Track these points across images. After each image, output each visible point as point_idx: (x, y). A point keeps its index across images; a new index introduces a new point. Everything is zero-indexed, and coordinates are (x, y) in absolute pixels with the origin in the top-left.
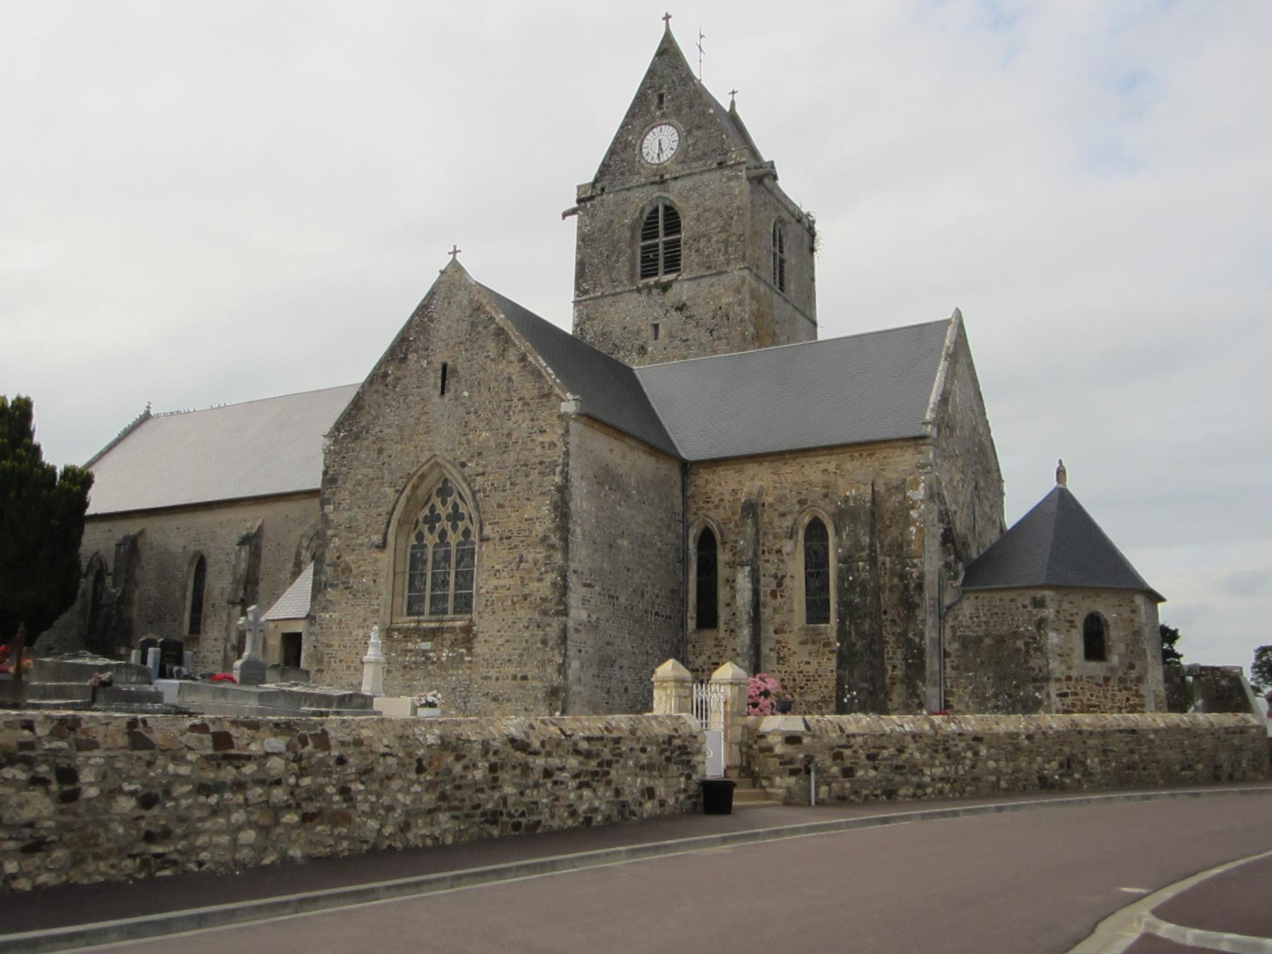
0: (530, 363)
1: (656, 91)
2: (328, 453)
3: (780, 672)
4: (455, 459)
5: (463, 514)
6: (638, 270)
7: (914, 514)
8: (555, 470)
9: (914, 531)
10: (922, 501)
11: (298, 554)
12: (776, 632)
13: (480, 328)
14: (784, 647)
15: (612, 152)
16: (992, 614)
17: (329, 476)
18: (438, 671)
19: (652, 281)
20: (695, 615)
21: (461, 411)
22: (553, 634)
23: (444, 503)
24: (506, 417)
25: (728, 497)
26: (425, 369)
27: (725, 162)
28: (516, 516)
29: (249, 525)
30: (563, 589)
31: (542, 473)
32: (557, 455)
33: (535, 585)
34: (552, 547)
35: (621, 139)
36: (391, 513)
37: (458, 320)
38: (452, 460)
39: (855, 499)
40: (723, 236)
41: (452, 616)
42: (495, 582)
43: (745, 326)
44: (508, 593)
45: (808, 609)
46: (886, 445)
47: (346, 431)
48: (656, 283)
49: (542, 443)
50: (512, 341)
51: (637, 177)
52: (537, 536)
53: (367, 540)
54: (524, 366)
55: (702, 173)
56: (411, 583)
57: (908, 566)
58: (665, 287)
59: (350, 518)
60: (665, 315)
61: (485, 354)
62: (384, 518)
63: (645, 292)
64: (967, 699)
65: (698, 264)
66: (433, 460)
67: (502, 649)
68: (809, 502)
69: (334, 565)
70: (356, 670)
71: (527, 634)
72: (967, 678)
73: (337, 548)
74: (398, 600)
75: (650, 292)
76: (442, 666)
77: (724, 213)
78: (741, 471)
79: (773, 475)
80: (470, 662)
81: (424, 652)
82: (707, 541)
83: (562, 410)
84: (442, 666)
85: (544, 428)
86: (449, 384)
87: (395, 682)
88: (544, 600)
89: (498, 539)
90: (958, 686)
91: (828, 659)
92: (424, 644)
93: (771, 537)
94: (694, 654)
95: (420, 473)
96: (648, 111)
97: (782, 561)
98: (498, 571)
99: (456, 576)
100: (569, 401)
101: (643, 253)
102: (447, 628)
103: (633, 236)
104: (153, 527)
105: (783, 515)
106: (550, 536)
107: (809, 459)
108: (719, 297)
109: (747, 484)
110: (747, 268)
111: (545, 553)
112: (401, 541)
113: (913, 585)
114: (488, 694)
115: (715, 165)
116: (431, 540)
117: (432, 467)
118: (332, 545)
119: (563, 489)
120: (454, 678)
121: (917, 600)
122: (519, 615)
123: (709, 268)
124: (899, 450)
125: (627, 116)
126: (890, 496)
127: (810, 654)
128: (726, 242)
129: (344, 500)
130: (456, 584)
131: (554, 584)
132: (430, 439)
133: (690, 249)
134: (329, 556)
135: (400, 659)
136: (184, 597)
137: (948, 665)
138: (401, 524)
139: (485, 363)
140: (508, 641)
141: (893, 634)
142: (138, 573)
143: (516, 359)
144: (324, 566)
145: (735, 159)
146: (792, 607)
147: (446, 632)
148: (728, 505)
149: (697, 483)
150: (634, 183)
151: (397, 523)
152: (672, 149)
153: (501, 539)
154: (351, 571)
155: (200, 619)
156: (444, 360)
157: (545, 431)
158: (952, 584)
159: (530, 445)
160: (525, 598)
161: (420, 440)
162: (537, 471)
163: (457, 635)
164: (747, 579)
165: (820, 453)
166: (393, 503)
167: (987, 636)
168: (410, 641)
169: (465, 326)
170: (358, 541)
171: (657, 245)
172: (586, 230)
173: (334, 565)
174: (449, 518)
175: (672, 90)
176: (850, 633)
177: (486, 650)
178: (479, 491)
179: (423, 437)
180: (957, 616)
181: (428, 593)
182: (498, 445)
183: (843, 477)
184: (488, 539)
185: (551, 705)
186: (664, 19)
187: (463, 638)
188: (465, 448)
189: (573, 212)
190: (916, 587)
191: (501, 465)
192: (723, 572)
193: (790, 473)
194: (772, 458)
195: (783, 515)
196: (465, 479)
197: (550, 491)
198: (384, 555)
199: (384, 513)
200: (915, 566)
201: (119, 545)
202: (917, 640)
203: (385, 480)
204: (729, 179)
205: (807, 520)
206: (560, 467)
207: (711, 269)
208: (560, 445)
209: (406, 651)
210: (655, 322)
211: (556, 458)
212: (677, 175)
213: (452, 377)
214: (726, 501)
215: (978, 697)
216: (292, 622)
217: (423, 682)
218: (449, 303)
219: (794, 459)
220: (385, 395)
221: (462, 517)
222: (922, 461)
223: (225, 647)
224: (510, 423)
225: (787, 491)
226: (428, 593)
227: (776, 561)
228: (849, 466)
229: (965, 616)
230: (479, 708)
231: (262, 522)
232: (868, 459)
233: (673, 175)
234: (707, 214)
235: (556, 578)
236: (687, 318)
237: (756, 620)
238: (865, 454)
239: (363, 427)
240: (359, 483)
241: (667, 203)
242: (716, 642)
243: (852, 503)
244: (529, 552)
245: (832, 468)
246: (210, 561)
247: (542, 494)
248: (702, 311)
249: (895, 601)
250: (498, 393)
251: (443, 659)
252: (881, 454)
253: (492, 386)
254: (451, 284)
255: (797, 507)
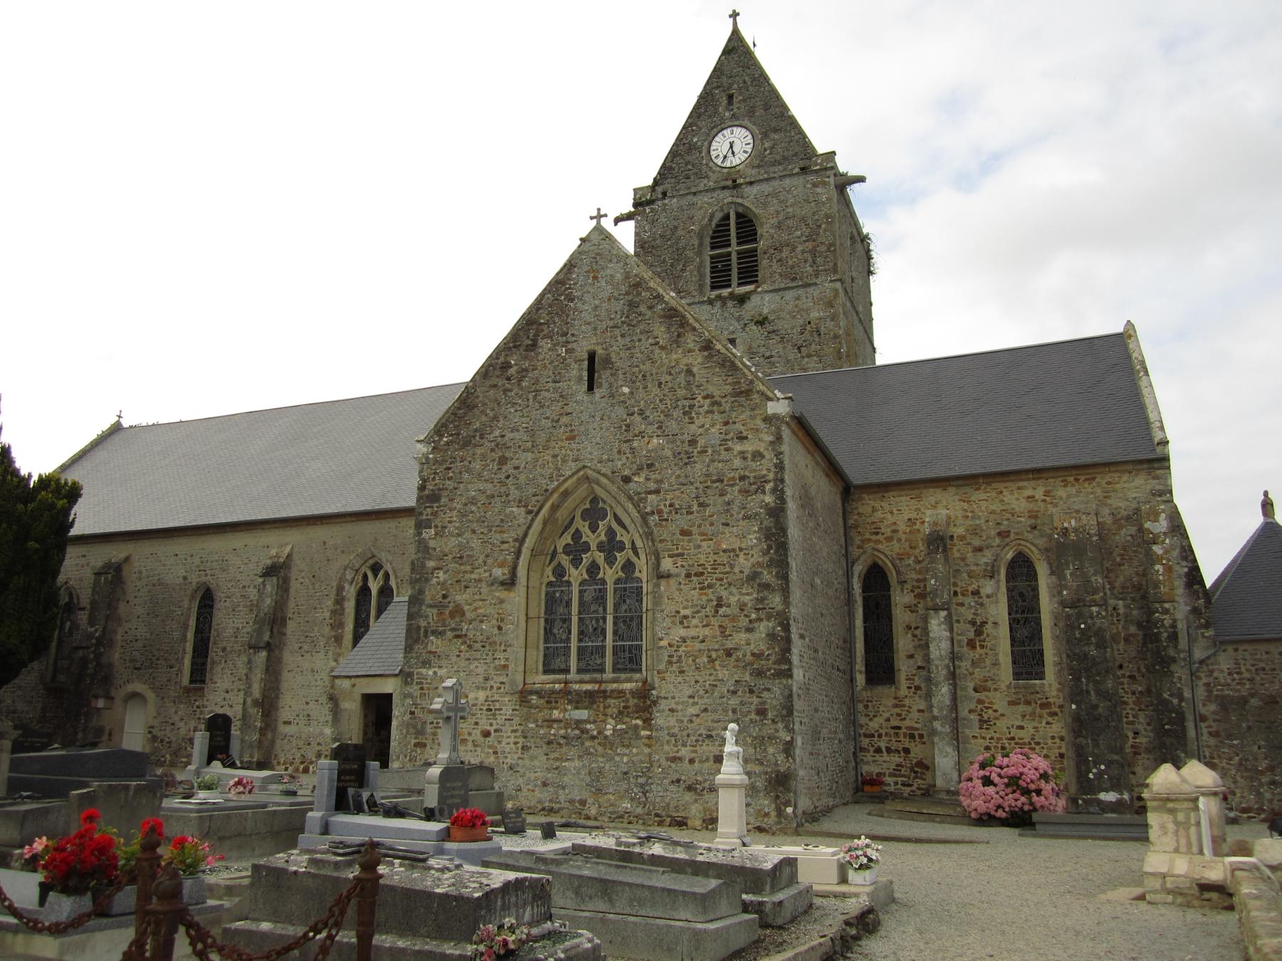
0: (719, 351)
1: (724, 91)
2: (424, 462)
3: (984, 738)
4: (613, 473)
5: (622, 542)
6: (708, 281)
7: (1157, 549)
8: (764, 487)
9: (1161, 570)
10: (1165, 533)
11: (340, 589)
12: (976, 690)
13: (643, 308)
14: (987, 708)
15: (674, 153)
16: (1257, 670)
17: (427, 492)
18: (600, 749)
19: (725, 292)
20: (863, 669)
21: (620, 412)
22: (774, 703)
23: (594, 528)
24: (687, 420)
25: (902, 527)
26: (565, 359)
27: (810, 166)
28: (709, 547)
29: (273, 552)
30: (783, 643)
31: (745, 492)
32: (765, 467)
33: (743, 636)
34: (766, 586)
35: (685, 141)
36: (521, 541)
37: (609, 300)
38: (609, 473)
39: (1076, 530)
40: (810, 245)
41: (611, 675)
42: (682, 632)
43: (840, 343)
44: (703, 646)
45: (1014, 663)
46: (1112, 469)
47: (452, 435)
48: (731, 294)
49: (742, 452)
50: (689, 324)
51: (705, 181)
52: (741, 572)
53: (487, 574)
54: (710, 356)
55: (781, 178)
56: (548, 632)
57: (1158, 612)
58: (742, 300)
59: (460, 545)
60: (743, 329)
61: (651, 341)
62: (511, 546)
63: (718, 304)
64: (1233, 772)
65: (781, 275)
66: (582, 473)
67: (697, 721)
68: (1012, 535)
69: (439, 606)
70: (475, 746)
71: (734, 702)
72: (1231, 746)
73: (442, 584)
74: (532, 653)
75: (724, 304)
76: (606, 742)
77: (810, 221)
78: (918, 497)
79: (962, 503)
80: (649, 737)
81: (578, 722)
82: (876, 580)
83: (770, 411)
84: (606, 742)
85: (744, 434)
86: (600, 377)
87: (536, 763)
88: (758, 656)
89: (683, 575)
90: (1219, 757)
91: (1048, 723)
92: (577, 712)
93: (965, 575)
94: (867, 715)
95: (562, 489)
96: (716, 112)
97: (982, 605)
98: (685, 617)
99: (615, 624)
100: (778, 399)
101: (712, 263)
102: (612, 691)
103: (701, 245)
104: (143, 558)
105: (979, 549)
106: (762, 573)
107: (1008, 484)
108: (807, 310)
109: (928, 512)
110: (840, 280)
111: (755, 596)
112: (535, 576)
113: (1165, 635)
114: (678, 781)
115: (797, 170)
116: (576, 575)
117: (579, 482)
118: (435, 580)
119: (777, 512)
120: (625, 759)
121: (1171, 652)
122: (720, 676)
123: (794, 279)
124: (1127, 475)
125: (690, 116)
126: (1120, 527)
127: (1024, 716)
128: (813, 252)
129: (449, 522)
130: (615, 633)
131: (772, 636)
132: (574, 446)
133: (770, 259)
134: (432, 593)
135: (542, 732)
136: (184, 639)
137: (1205, 731)
138: (534, 554)
139: (652, 352)
140: (706, 710)
141: (1133, 693)
142: (122, 608)
143: (697, 349)
144: (424, 607)
145: (820, 164)
146: (997, 660)
147: (610, 697)
148: (903, 537)
149: (860, 510)
150: (701, 187)
151: (529, 552)
152: (745, 152)
153: (688, 576)
154: (463, 614)
155: (204, 664)
156: (592, 347)
157: (746, 438)
158: (1203, 634)
159: (724, 454)
160: (729, 653)
161: (561, 447)
162: (737, 488)
163: (627, 701)
164: (943, 626)
165: (1024, 477)
166: (524, 527)
167: (1252, 696)
168: (556, 708)
169: (619, 306)
170: (473, 576)
171: (729, 254)
172: (645, 236)
173: (439, 606)
174: (601, 547)
175: (743, 90)
176: (1088, 692)
177: (672, 722)
178: (653, 513)
179: (566, 444)
180: (1212, 672)
181: (574, 644)
182: (676, 455)
183: (1056, 505)
184: (669, 576)
185: (777, 797)
186: (730, 16)
187: (636, 705)
188: (628, 458)
189: (628, 217)
190: (1169, 637)
191: (682, 480)
192: (901, 617)
193: (984, 501)
194: (961, 482)
195: (979, 549)
196: (630, 498)
197: (757, 514)
198: (512, 594)
199: (511, 540)
200: (1166, 612)
201: (98, 574)
202: (1175, 701)
203: (511, 498)
204: (815, 185)
205: (1010, 556)
206: (772, 484)
207: (795, 280)
208: (769, 455)
209: (550, 722)
210: (731, 337)
211: (764, 472)
212: (753, 180)
213: (605, 369)
214: (901, 532)
215: (1246, 770)
216: (378, 679)
217: (577, 763)
218: (595, 278)
219: (989, 484)
220: (505, 391)
221: (621, 547)
222: (1158, 487)
223: (245, 703)
224: (693, 427)
225: (983, 521)
226: (574, 644)
227: (973, 604)
228: (1061, 493)
229: (1222, 671)
230: (667, 800)
231: (292, 549)
232: (1086, 485)
233: (748, 180)
234: (790, 222)
235: (774, 628)
236: (769, 333)
237: (953, 676)
238: (1082, 478)
239: (476, 430)
240: (473, 501)
241: (740, 210)
242: (896, 702)
243: (1072, 536)
244: (731, 593)
245: (1039, 493)
246: (219, 595)
247: (746, 517)
248: (784, 325)
249: (1133, 654)
250: (673, 390)
251: (608, 733)
252: (1102, 480)
253: (663, 380)
254: (598, 254)
255: (997, 541)
